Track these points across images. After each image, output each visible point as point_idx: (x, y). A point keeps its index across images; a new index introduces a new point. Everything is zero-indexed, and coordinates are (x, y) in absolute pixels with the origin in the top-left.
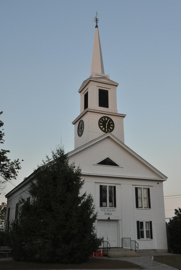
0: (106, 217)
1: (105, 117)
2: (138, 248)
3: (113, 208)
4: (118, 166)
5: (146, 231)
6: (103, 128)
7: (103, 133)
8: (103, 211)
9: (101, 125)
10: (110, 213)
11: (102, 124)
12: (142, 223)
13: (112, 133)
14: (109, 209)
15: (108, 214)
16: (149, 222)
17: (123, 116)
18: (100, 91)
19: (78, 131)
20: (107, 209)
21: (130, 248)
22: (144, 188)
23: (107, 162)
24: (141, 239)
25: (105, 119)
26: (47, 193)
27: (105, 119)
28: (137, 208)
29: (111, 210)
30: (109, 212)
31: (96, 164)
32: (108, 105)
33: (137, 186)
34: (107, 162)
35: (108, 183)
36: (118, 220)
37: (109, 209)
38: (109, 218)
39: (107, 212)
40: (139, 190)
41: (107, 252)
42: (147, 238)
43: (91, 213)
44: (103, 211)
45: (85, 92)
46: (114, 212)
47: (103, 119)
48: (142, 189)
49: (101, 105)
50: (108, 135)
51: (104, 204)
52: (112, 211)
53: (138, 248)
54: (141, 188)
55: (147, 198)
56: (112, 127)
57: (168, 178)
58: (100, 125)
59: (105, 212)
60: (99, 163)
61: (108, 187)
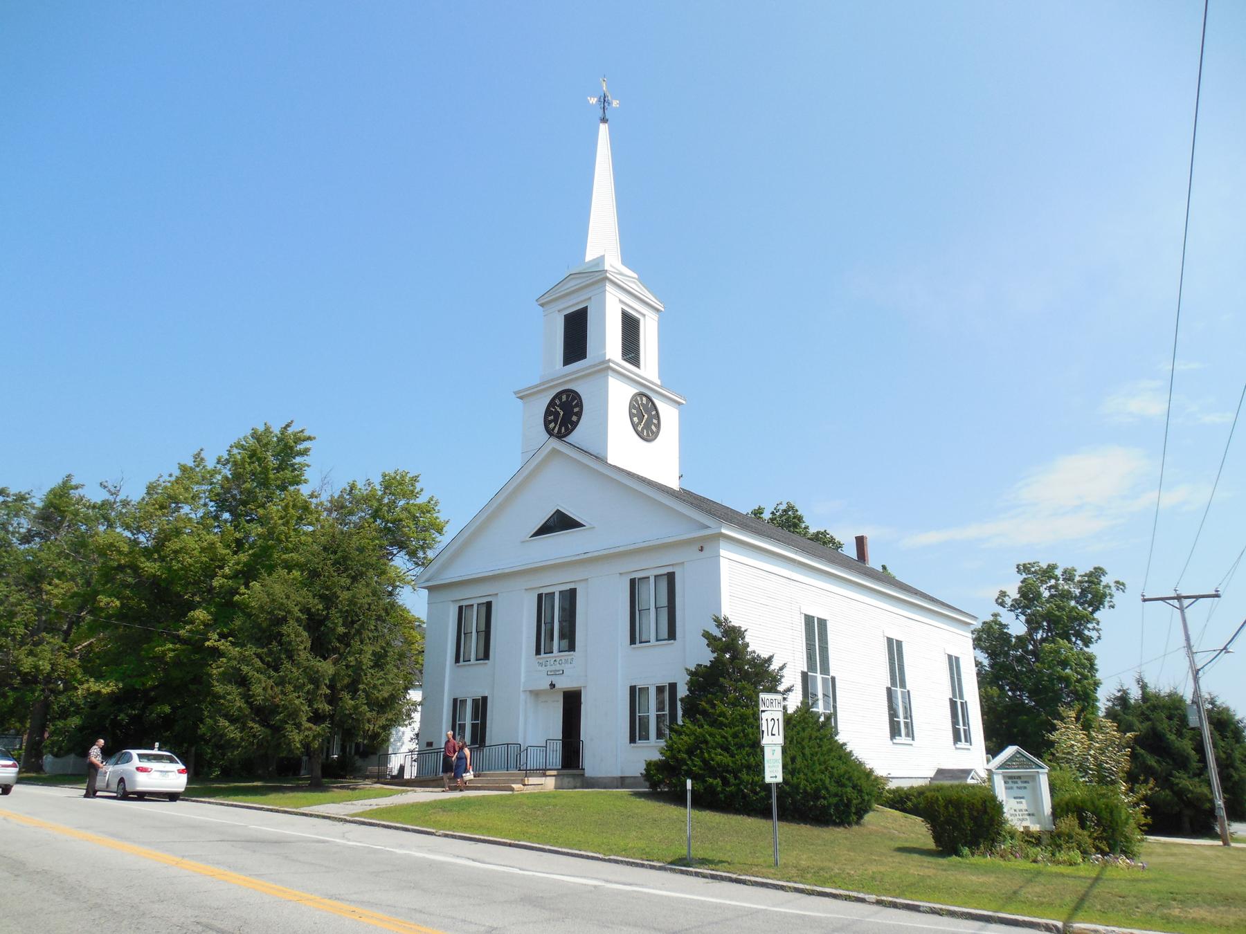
10: (559, 671)
16: (667, 684)
23: (560, 523)
24: (640, 743)
26: (299, 573)
30: (558, 667)
32: (565, 329)
34: (560, 523)
35: (556, 584)
37: (563, 659)
39: (553, 668)
43: (1071, 923)
45: (637, 311)
52: (566, 661)
56: (560, 399)
59: (549, 668)
60: (537, 534)
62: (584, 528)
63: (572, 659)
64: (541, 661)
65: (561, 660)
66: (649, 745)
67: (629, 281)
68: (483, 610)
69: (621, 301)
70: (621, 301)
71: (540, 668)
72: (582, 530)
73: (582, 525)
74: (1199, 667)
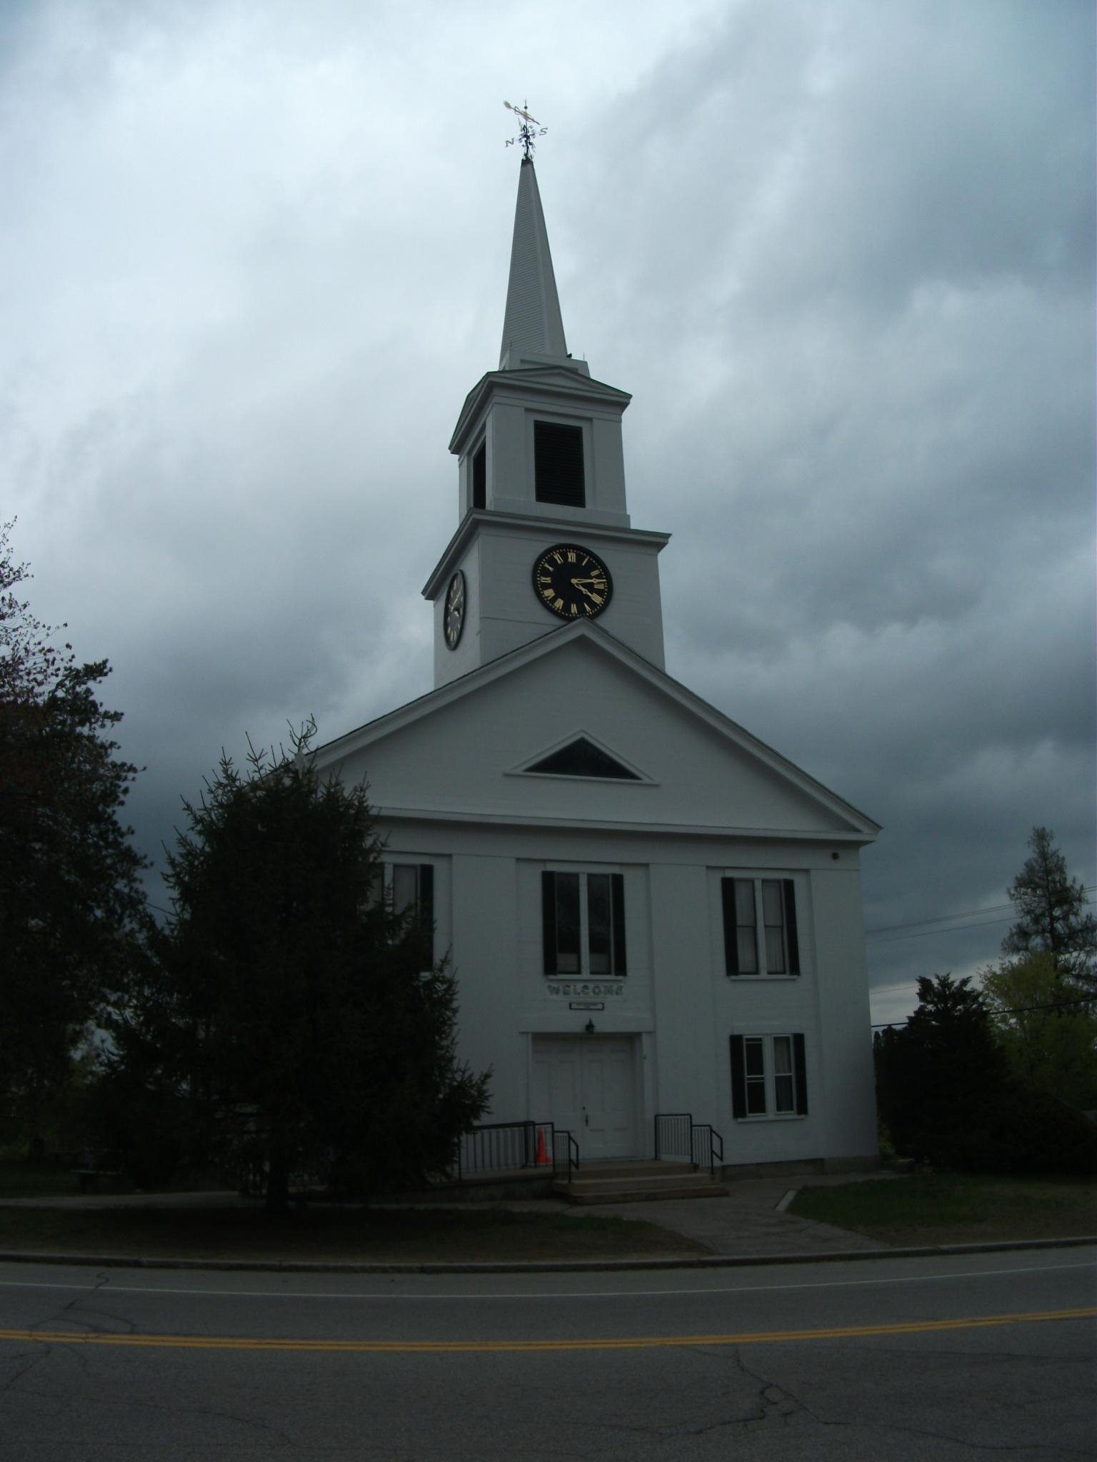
0: (573, 1022)
1: (563, 549)
2: (721, 1159)
3: (612, 977)
4: (632, 776)
5: (777, 1078)
6: (554, 600)
7: (555, 621)
8: (561, 993)
9: (546, 586)
10: (595, 1004)
11: (548, 580)
12: (755, 1047)
13: (603, 621)
14: (591, 986)
15: (588, 1007)
17: (656, 542)
18: (541, 429)
19: (446, 625)
20: (579, 986)
21: (686, 1159)
22: (764, 881)
24: (752, 1117)
25: (565, 556)
27: (565, 556)
28: (733, 977)
29: (602, 989)
31: (519, 771)
33: (729, 874)
36: (639, 1034)
37: (591, 986)
38: (590, 1027)
40: (741, 895)
41: (565, 1182)
42: (779, 1108)
44: (561, 993)
46: (615, 996)
47: (557, 557)
48: (758, 885)
49: (544, 494)
50: (580, 629)
51: (563, 959)
52: (609, 991)
53: (721, 1159)
54: (752, 881)
55: (782, 927)
57: (880, 828)
58: (538, 589)
60: (871, 842)
61: (583, 882)
62: (640, 782)
63: (620, 988)
64: (554, 985)
65: (598, 987)
66: (764, 1119)
67: (533, 376)
68: (744, 956)
69: (528, 410)
70: (528, 410)
71: (554, 997)
72: (633, 784)
73: (638, 778)
74: (203, 807)
